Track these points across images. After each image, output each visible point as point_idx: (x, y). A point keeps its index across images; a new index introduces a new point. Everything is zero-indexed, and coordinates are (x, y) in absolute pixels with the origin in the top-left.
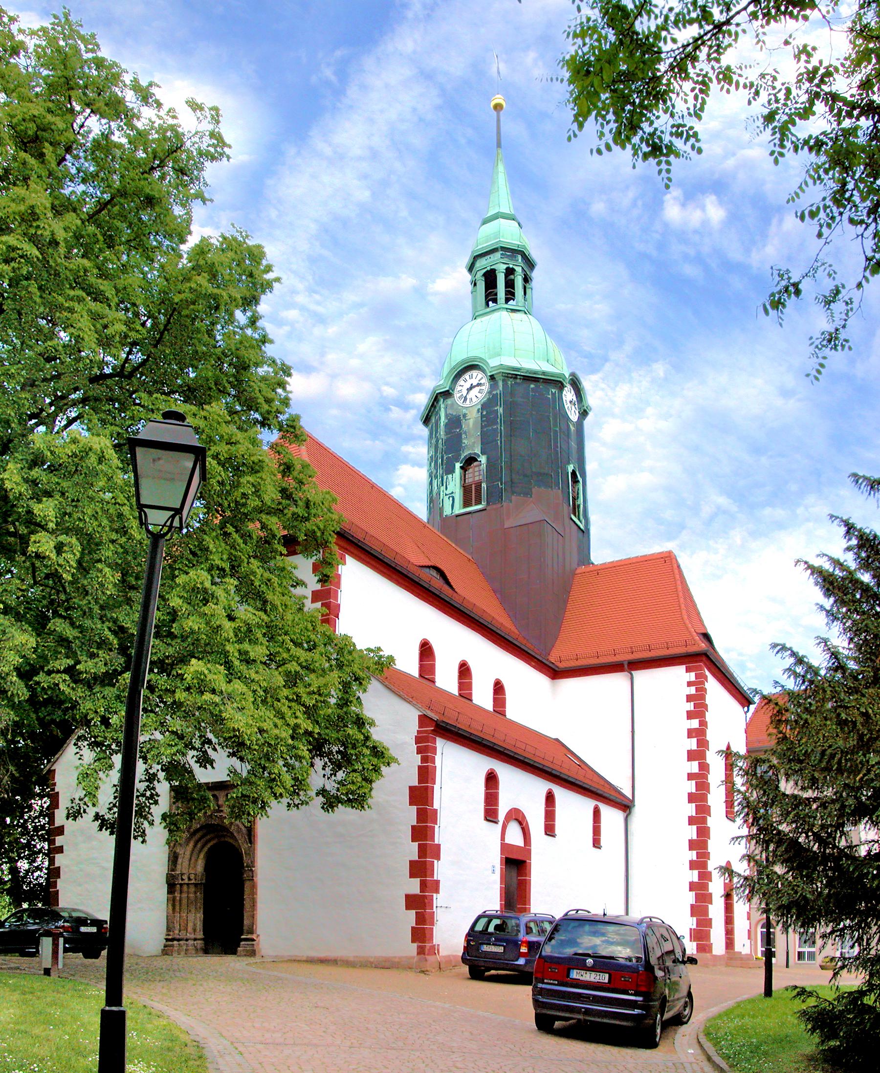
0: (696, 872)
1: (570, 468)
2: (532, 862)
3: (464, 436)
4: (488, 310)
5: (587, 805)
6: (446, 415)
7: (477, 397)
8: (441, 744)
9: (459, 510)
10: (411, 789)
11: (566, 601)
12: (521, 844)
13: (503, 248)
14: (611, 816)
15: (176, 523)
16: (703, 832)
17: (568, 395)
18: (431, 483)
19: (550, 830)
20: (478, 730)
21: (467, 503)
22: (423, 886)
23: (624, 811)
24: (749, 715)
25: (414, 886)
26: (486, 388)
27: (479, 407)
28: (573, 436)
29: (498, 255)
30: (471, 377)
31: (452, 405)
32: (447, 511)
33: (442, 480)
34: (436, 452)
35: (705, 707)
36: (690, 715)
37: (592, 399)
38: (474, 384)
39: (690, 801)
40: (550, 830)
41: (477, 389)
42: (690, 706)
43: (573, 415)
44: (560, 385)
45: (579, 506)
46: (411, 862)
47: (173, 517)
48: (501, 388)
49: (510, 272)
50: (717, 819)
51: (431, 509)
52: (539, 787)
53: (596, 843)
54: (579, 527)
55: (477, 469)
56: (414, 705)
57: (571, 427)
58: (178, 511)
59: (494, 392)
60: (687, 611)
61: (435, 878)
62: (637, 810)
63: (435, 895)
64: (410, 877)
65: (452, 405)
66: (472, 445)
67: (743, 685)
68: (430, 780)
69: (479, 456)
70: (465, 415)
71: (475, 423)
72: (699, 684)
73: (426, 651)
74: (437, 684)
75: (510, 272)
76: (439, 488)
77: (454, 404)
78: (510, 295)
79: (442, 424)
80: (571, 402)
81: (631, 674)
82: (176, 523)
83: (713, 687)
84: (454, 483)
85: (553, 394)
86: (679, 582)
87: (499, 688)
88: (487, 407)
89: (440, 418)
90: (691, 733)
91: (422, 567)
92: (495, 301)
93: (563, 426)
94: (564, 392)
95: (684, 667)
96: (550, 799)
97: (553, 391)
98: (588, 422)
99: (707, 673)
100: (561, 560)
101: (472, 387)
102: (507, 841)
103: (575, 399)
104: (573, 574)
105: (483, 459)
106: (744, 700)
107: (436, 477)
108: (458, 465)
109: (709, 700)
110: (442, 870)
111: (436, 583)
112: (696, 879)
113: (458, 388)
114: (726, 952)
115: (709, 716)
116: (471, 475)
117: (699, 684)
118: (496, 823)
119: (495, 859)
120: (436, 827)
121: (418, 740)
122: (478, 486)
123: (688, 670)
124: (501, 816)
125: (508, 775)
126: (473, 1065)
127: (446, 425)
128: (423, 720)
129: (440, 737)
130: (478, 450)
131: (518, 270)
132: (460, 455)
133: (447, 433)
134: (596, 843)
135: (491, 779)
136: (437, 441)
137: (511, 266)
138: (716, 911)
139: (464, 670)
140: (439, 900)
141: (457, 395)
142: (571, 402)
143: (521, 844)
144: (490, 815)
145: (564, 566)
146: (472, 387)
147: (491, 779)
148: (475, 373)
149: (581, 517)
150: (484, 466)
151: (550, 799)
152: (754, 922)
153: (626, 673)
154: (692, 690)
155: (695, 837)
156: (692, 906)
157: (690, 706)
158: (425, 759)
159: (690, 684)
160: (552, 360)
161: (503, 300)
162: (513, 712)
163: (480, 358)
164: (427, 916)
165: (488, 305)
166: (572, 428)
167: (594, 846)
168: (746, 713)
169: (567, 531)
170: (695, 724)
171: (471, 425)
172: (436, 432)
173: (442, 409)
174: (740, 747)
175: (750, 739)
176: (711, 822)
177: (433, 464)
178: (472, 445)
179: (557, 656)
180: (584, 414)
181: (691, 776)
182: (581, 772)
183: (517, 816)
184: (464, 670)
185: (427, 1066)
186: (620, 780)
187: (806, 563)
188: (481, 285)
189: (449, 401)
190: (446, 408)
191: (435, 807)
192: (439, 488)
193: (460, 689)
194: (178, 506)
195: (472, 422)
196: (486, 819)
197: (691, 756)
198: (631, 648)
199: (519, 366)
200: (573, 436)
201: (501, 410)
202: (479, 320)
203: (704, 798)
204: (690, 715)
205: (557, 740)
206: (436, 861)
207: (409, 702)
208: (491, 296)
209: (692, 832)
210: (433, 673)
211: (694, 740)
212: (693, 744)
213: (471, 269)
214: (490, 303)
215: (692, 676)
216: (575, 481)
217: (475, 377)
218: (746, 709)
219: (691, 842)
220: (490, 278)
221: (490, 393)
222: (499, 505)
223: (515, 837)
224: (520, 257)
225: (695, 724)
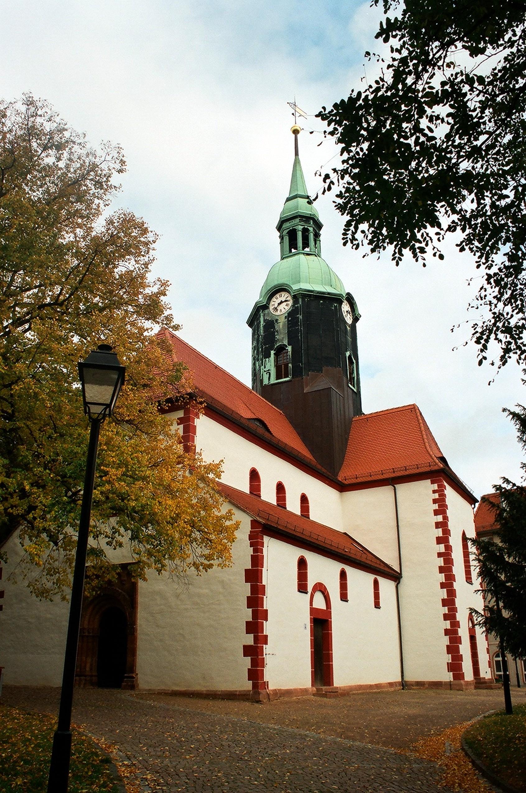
0: (448, 622)
1: (348, 354)
2: (332, 620)
3: (276, 333)
4: (291, 254)
5: (368, 578)
6: (265, 320)
7: (284, 309)
8: (266, 540)
9: (273, 381)
10: (247, 571)
11: (347, 440)
12: (325, 608)
13: (300, 216)
14: (387, 586)
15: (107, 412)
16: (452, 593)
17: (345, 307)
18: (254, 364)
19: (344, 597)
20: (292, 530)
21: (278, 377)
22: (256, 639)
23: (395, 581)
24: (475, 509)
25: (249, 640)
26: (290, 303)
27: (286, 315)
28: (349, 334)
29: (297, 220)
30: (281, 296)
31: (268, 313)
32: (266, 382)
33: (262, 362)
34: (258, 343)
35: (446, 506)
36: (436, 513)
37: (361, 309)
38: (283, 300)
39: (441, 572)
40: (344, 597)
41: (285, 303)
42: (436, 507)
43: (349, 320)
44: (341, 302)
45: (354, 378)
46: (247, 623)
47: (105, 409)
48: (301, 303)
49: (305, 231)
50: (460, 584)
51: (254, 381)
52: (335, 567)
53: (377, 605)
54: (353, 390)
55: (285, 355)
56: (247, 513)
57: (348, 327)
58: (108, 406)
59: (296, 306)
60: (429, 443)
61: (265, 634)
62: (404, 580)
63: (264, 646)
64: (247, 633)
65: (268, 313)
66: (282, 338)
67: (469, 490)
68: (260, 565)
69: (287, 346)
70: (277, 320)
71: (283, 326)
72: (440, 491)
73: (254, 475)
74: (262, 498)
75: (305, 231)
76: (260, 367)
77: (269, 313)
78: (306, 244)
79: (261, 326)
80: (347, 312)
81: (395, 487)
82: (107, 412)
83: (450, 493)
84: (270, 364)
85: (335, 307)
86: (422, 425)
87: (304, 499)
88: (291, 315)
89: (260, 322)
90: (438, 525)
91: (250, 419)
92: (296, 248)
93: (343, 328)
94: (343, 306)
95: (429, 480)
96: (343, 575)
97: (336, 305)
98: (358, 325)
99: (445, 484)
100: (342, 412)
101: (282, 302)
102: (314, 606)
103: (350, 310)
104: (351, 421)
105: (289, 348)
106: (471, 499)
107: (258, 360)
108: (272, 352)
109: (448, 501)
110: (269, 628)
111: (260, 430)
112: (449, 627)
113: (272, 303)
114: (475, 679)
115: (449, 513)
116: (281, 359)
117: (440, 491)
118: (306, 593)
119: (306, 619)
120: (265, 597)
121: (250, 537)
122: (286, 366)
123: (433, 483)
124: (310, 589)
125: (313, 559)
126: (302, 772)
127: (264, 327)
128: (254, 523)
129: (265, 535)
130: (286, 342)
131: (311, 229)
132: (274, 346)
133: (265, 332)
134: (377, 605)
135: (302, 563)
136: (258, 336)
137: (306, 227)
138: (465, 649)
139: (280, 488)
140: (267, 649)
141: (271, 308)
142: (347, 312)
143: (325, 608)
144: (302, 588)
145: (345, 416)
146: (282, 302)
147: (302, 563)
148: (283, 294)
149: (356, 385)
150: (290, 353)
151: (343, 575)
152: (491, 654)
153: (391, 486)
154: (436, 496)
155: (446, 597)
156: (447, 646)
157: (436, 507)
158: (255, 551)
159: (434, 492)
160: (334, 285)
161: (301, 248)
162: (314, 516)
163: (287, 284)
164: (259, 661)
165: (290, 251)
166: (348, 328)
167: (376, 607)
168: (473, 508)
169: (346, 392)
170: (440, 518)
171: (281, 327)
172: (258, 331)
173: (262, 317)
174: (472, 534)
175: (477, 526)
176: (456, 585)
177: (256, 352)
178: (282, 338)
179: (342, 476)
180: (356, 319)
181: (440, 555)
182: (364, 556)
183: (320, 588)
184: (280, 488)
185: (268, 772)
186: (389, 558)
187: (509, 411)
188: (286, 239)
189: (266, 311)
190: (264, 316)
191: (263, 584)
192: (260, 367)
193: (278, 500)
194: (108, 402)
195: (281, 325)
196: (299, 591)
197: (439, 540)
198: (393, 469)
199: (313, 289)
200: (349, 334)
201: (301, 317)
202: (285, 260)
203: (450, 570)
204: (436, 513)
205: (345, 534)
206: (265, 622)
207: (244, 511)
208: (293, 244)
209: (444, 594)
210: (260, 491)
211: (440, 530)
212: (439, 532)
213: (279, 228)
214: (293, 250)
215: (435, 486)
216: (351, 363)
217: (284, 296)
218: (473, 506)
219: (443, 600)
220: (292, 234)
221: (293, 306)
222: (300, 378)
223: (319, 603)
224: (312, 221)
225: (440, 518)
